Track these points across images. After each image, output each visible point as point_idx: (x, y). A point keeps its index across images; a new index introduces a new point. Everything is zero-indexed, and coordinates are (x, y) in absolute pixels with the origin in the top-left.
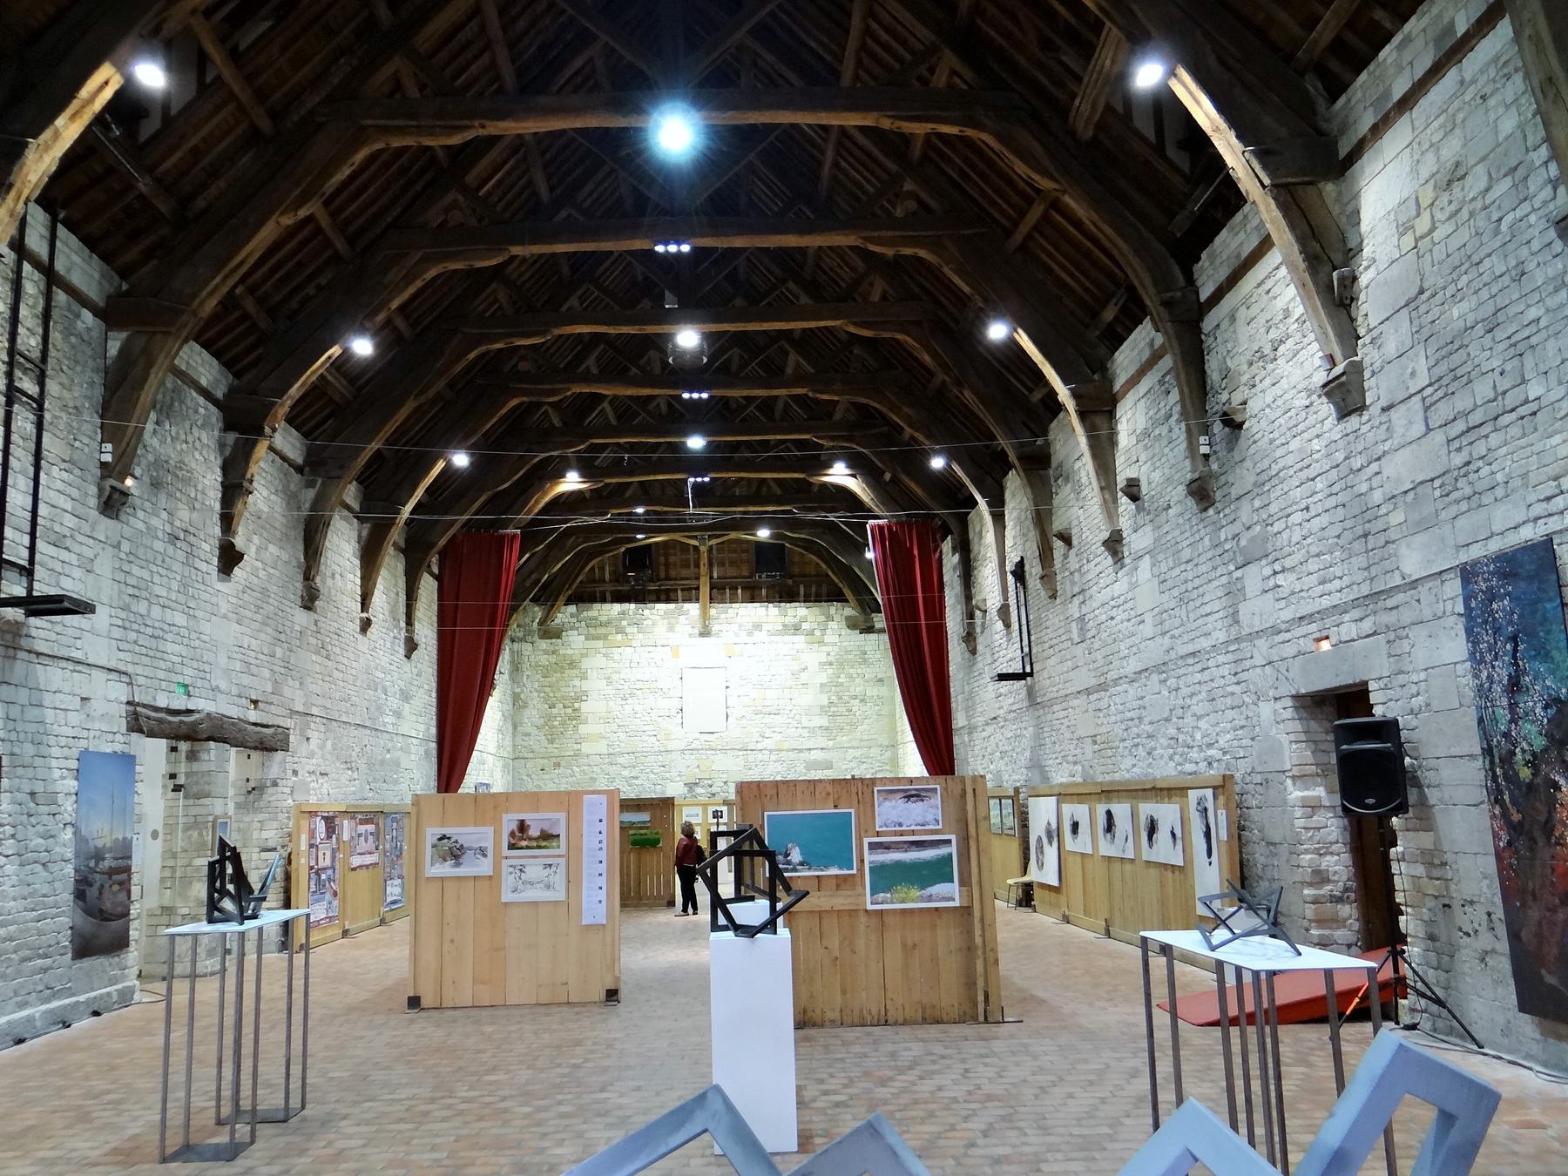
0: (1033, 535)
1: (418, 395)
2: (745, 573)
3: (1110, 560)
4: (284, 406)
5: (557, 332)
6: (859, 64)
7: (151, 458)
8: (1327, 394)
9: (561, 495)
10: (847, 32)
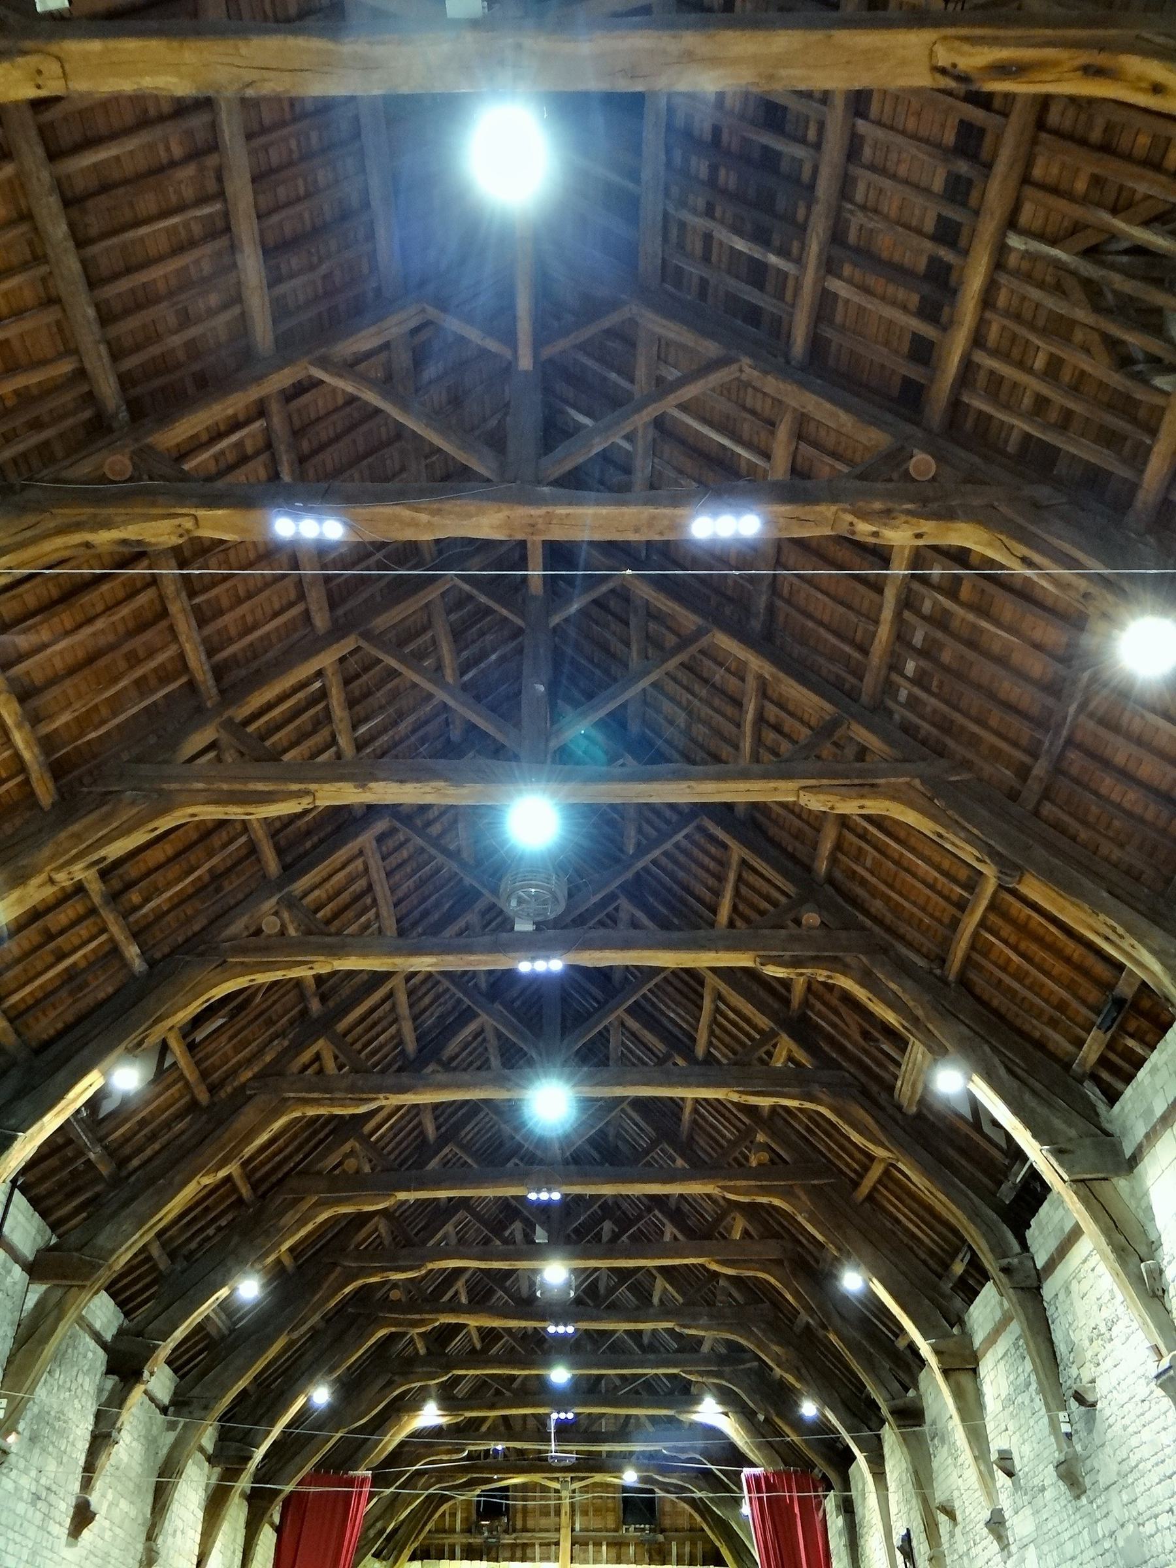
0: (915, 1503)
1: (292, 1330)
2: (611, 1524)
3: (996, 1546)
4: (166, 1349)
5: (430, 1266)
6: (712, 1033)
7: (36, 1409)
8: (1161, 1386)
9: (416, 1434)
10: (700, 1008)
